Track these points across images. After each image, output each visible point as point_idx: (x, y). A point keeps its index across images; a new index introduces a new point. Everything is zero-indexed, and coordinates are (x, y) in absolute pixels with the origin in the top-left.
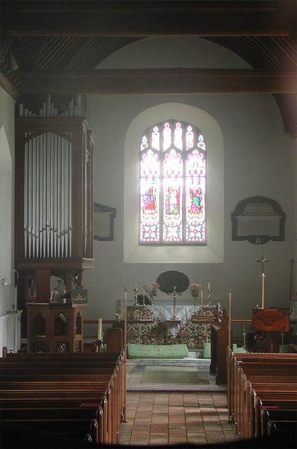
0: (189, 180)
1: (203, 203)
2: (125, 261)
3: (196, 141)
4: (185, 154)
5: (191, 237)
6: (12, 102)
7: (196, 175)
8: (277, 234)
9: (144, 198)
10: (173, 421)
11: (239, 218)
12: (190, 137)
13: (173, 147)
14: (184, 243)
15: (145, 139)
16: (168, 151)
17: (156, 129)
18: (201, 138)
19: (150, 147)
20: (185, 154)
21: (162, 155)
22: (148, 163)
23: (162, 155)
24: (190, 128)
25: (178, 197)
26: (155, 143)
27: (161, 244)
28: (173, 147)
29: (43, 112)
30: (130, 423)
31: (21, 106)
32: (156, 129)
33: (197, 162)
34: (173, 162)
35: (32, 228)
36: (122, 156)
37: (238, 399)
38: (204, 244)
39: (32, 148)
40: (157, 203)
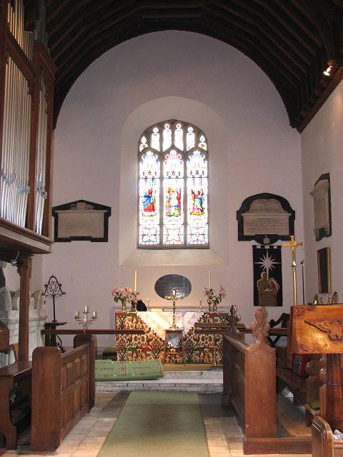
0: (190, 180)
3: (198, 141)
4: (185, 155)
7: (196, 176)
12: (191, 138)
16: (168, 151)
18: (202, 138)
20: (185, 155)
21: (162, 156)
22: (149, 163)
23: (162, 156)
25: (179, 199)
28: (173, 147)
33: (198, 163)
34: (174, 162)
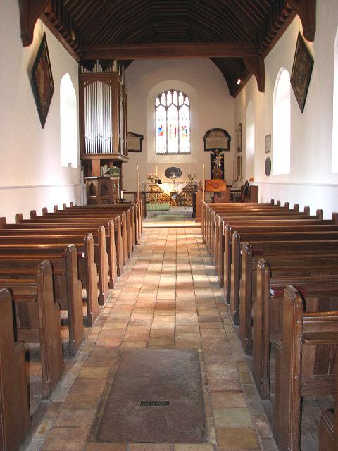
1: (188, 133)
2: (148, 162)
5: (182, 151)
6: (77, 65)
8: (227, 147)
9: (157, 130)
10: (169, 244)
11: (207, 139)
13: (172, 103)
14: (179, 153)
15: (158, 99)
17: (163, 94)
18: (187, 99)
19: (160, 104)
22: (160, 112)
24: (181, 94)
26: (163, 102)
27: (167, 154)
28: (172, 103)
29: (94, 70)
30: (142, 245)
31: (82, 67)
32: (163, 94)
33: (185, 111)
35: (91, 136)
36: (147, 109)
37: (166, 205)
38: (189, 154)
39: (87, 90)
40: (165, 133)
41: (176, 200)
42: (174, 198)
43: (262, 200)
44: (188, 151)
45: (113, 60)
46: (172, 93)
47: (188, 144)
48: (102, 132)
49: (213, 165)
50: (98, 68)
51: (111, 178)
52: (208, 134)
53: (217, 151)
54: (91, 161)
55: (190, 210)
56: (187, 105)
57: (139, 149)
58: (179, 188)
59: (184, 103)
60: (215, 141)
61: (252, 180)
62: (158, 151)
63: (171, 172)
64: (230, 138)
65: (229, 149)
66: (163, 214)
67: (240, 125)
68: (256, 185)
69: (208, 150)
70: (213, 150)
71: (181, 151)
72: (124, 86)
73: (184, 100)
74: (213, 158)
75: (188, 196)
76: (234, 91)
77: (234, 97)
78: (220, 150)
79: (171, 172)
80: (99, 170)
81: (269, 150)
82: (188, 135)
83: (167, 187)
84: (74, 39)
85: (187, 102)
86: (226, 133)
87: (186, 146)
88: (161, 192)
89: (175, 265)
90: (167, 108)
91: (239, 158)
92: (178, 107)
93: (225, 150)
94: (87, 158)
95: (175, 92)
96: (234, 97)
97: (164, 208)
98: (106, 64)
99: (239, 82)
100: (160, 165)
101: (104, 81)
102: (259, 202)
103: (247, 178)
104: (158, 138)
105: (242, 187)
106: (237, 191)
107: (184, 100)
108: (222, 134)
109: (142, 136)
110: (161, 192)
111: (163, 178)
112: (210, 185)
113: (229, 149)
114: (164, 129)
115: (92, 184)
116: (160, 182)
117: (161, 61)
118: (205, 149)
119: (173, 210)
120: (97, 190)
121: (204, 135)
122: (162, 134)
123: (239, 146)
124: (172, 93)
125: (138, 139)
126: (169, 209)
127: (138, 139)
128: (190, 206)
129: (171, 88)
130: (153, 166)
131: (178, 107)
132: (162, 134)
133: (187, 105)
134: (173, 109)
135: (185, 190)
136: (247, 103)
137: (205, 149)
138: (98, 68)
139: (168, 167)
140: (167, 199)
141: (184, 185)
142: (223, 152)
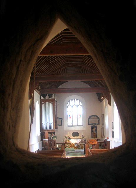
1: (82, 117)
6: (39, 96)
8: (98, 123)
9: (68, 116)
14: (78, 126)
15: (68, 103)
18: (81, 102)
24: (78, 101)
29: (46, 98)
32: (71, 101)
35: (45, 123)
37: (73, 149)
38: (82, 126)
39: (43, 105)
40: (71, 117)
41: (77, 146)
42: (76, 145)
43: (111, 148)
44: (81, 125)
45: (53, 94)
46: (74, 100)
47: (82, 122)
48: (49, 121)
49: (92, 131)
50: (47, 97)
51: (54, 140)
52: (90, 117)
53: (94, 125)
54: (45, 133)
55: (83, 151)
56: (81, 105)
57: (61, 124)
58: (78, 141)
59: (80, 105)
60: (93, 121)
61: (108, 138)
62: (69, 125)
63: (75, 134)
64: (99, 119)
65: (99, 124)
66: (72, 152)
67: (103, 114)
68: (109, 141)
69: (90, 124)
70: (92, 124)
71: (79, 125)
72: (56, 102)
73: (80, 103)
74: (92, 128)
75: (82, 144)
76: (101, 101)
77: (101, 102)
78: (95, 124)
79: (75, 134)
80: (47, 135)
81: (113, 128)
82: (82, 118)
83: (73, 141)
84: (40, 88)
85: (81, 104)
86: (98, 117)
87: (81, 122)
88: (71, 143)
89: (75, 140)
90: (72, 106)
91: (103, 128)
92: (77, 106)
93: (97, 124)
94: (43, 131)
95: (76, 100)
96: (101, 102)
97: (72, 150)
98: (50, 96)
99: (102, 98)
100: (70, 131)
101: (50, 102)
102: (110, 148)
103: (106, 137)
104: (69, 119)
105: (104, 141)
106: (103, 142)
107: (80, 103)
108: (95, 117)
109: (62, 119)
110: (71, 143)
111: (71, 137)
112: (91, 142)
113: (99, 124)
114: (71, 116)
115: (46, 142)
116: (70, 139)
117: (72, 93)
118: (89, 124)
119: (76, 151)
120: (48, 144)
121: (88, 118)
122: (70, 118)
123: (103, 123)
124: (74, 100)
125: (60, 120)
126: (74, 150)
127: (61, 124)
128: (83, 149)
129: (74, 98)
130: (67, 132)
131: (77, 106)
132: (70, 118)
133: (81, 105)
134: (75, 107)
135: (81, 142)
136: (105, 107)
137: (89, 124)
138: (47, 97)
139: (74, 132)
140: (73, 146)
141: (80, 140)
142: (97, 125)
